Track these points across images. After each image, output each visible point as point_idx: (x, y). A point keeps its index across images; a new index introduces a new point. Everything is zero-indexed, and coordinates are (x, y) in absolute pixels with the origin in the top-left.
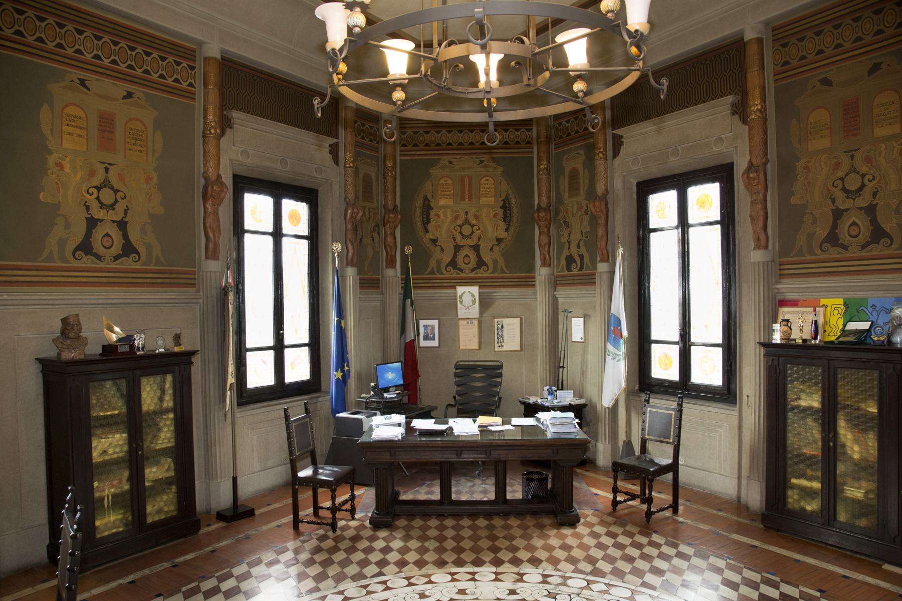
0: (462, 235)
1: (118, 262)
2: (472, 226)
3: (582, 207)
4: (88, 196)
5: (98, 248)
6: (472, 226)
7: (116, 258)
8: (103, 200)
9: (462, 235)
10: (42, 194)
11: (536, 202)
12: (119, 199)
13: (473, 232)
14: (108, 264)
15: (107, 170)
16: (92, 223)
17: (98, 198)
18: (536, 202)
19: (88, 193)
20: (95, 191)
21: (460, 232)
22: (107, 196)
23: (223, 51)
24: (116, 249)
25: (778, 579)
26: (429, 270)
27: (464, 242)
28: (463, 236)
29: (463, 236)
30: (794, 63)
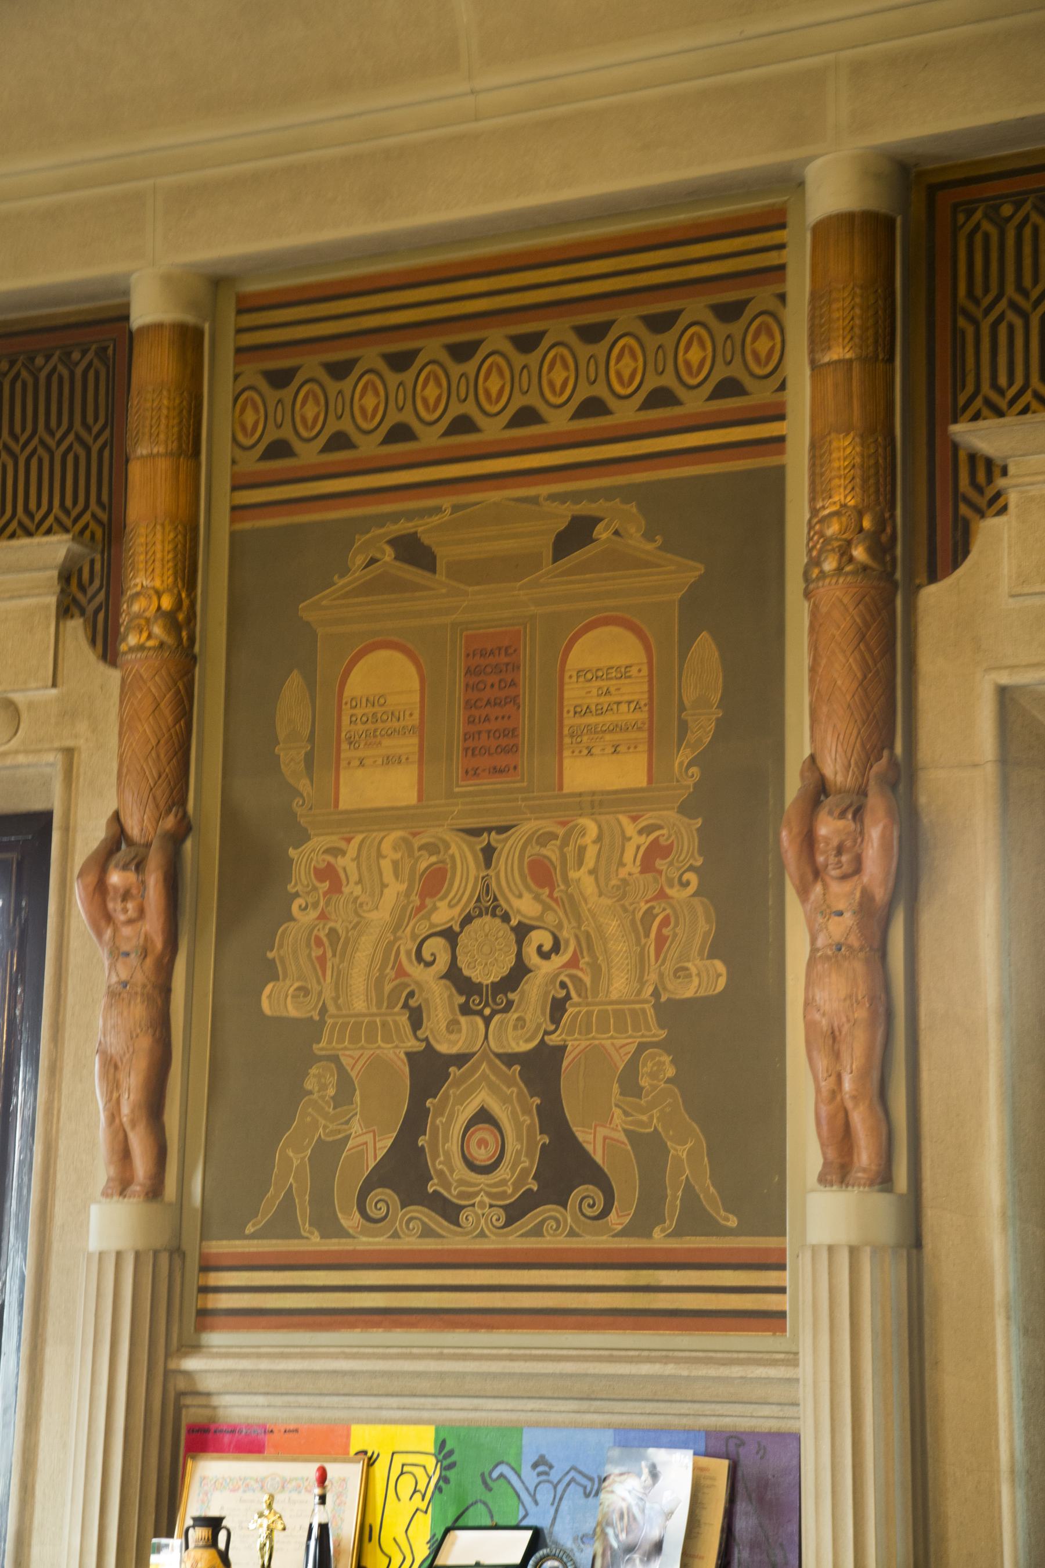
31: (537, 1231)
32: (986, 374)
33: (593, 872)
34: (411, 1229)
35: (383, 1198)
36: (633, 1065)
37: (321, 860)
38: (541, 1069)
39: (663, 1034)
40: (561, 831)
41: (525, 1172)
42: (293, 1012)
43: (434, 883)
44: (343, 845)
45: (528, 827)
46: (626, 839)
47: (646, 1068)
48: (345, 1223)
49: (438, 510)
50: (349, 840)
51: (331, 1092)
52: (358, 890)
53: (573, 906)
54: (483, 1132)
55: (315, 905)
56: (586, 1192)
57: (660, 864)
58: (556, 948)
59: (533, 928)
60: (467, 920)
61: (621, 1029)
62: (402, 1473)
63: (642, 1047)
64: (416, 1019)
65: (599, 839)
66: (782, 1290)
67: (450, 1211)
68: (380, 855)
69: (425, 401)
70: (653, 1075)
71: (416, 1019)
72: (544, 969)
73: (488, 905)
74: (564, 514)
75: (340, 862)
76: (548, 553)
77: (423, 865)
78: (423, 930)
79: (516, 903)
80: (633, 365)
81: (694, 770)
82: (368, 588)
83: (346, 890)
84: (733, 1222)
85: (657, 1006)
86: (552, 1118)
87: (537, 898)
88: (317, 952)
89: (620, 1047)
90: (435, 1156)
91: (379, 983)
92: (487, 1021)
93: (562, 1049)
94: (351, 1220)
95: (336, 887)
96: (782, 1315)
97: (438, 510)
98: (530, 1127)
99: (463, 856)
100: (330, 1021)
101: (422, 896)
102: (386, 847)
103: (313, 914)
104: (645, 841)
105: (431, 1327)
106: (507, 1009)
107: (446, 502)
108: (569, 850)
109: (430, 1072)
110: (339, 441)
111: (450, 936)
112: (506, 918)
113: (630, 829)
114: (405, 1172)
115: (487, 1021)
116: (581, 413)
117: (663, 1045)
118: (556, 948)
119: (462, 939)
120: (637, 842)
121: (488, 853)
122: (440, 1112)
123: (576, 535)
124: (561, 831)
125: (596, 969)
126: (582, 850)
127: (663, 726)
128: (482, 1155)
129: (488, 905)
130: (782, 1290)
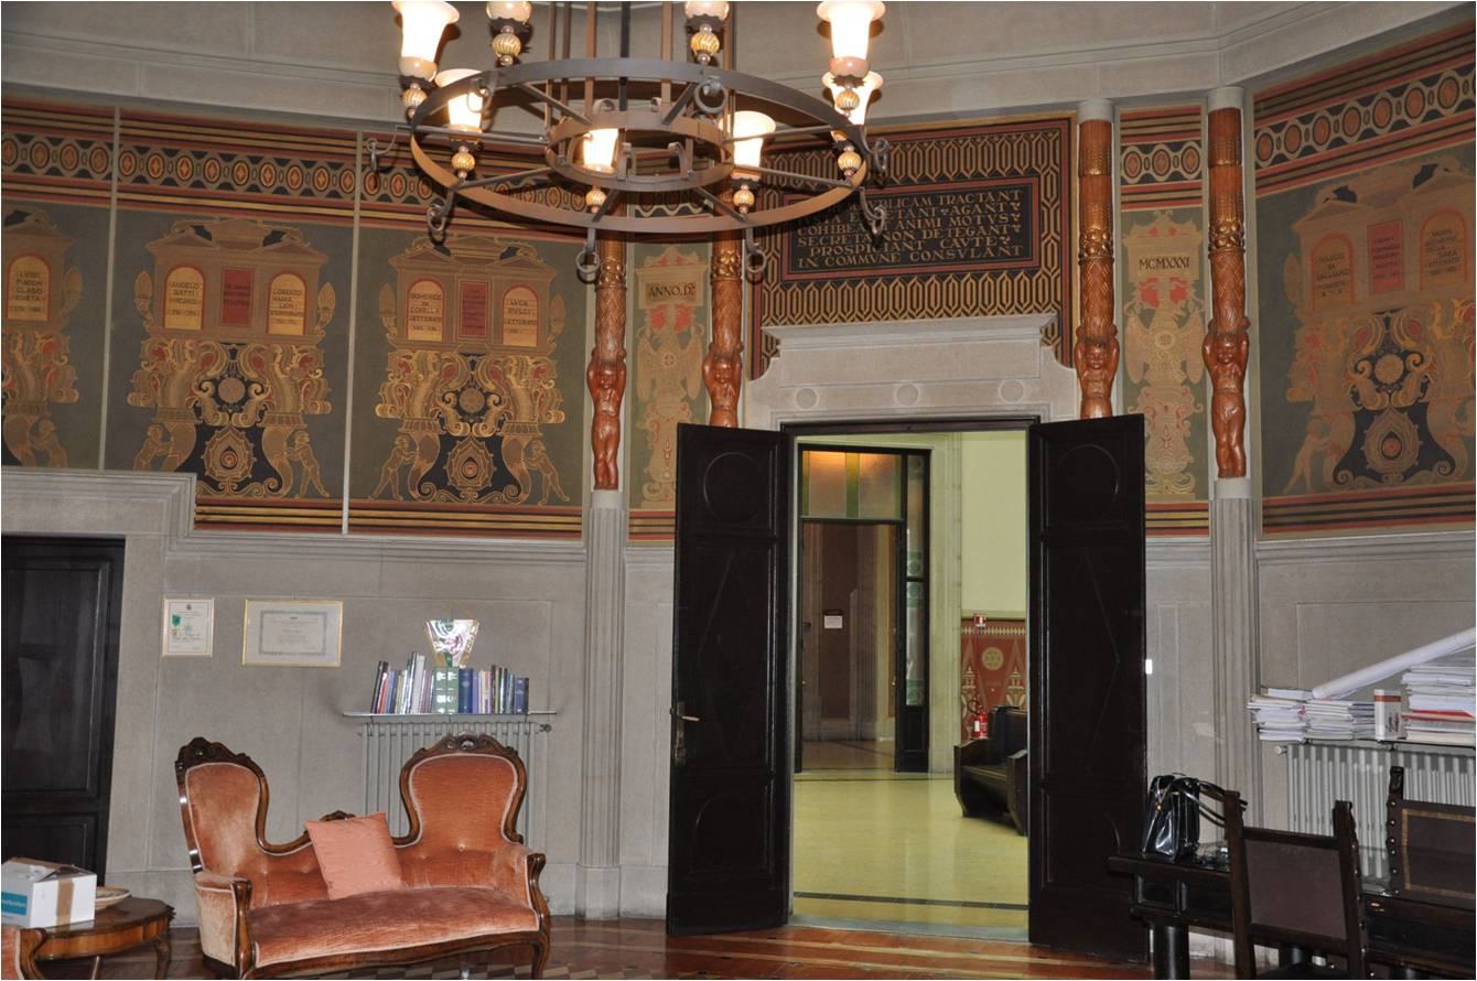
0: (1376, 381)
1: (1413, 479)
2: (1404, 355)
3: (700, 331)
4: (442, 405)
5: (1374, 458)
6: (1404, 355)
7: (1407, 475)
8: (1380, 378)
9: (1376, 381)
10: (379, 406)
11: (590, 344)
12: (491, 403)
13: (1406, 372)
14: (1392, 485)
15: (1387, 322)
16: (1364, 418)
17: (1372, 377)
18: (590, 344)
19: (444, 400)
20: (1365, 364)
21: (1372, 377)
22: (1390, 368)
23: (1114, 104)
24: (1409, 458)
25: (511, 966)
26: (1293, 481)
27: (219, 419)
28: (1380, 386)
29: (1380, 386)
30: (68, 176)
31: (490, 501)
32: (773, 245)
33: (515, 375)
34: (441, 497)
35: (428, 486)
36: (529, 445)
37: (156, 347)
38: (254, 434)
39: (305, 426)
40: (502, 360)
41: (246, 471)
42: (390, 416)
43: (208, 361)
44: (412, 354)
45: (252, 347)
46: (294, 354)
47: (534, 447)
48: (413, 495)
49: (212, 218)
50: (169, 340)
51: (160, 436)
52: (173, 360)
53: (508, 387)
54: (471, 464)
55: (399, 377)
56: (511, 489)
57: (307, 364)
58: (500, 402)
59: (253, 382)
60: (463, 389)
61: (288, 423)
62: (1256, 566)
63: (296, 430)
64: (442, 421)
65: (517, 365)
66: (1207, 519)
67: (457, 493)
68: (184, 348)
69: (182, 172)
70: (300, 440)
71: (442, 421)
72: (496, 410)
73: (472, 383)
74: (269, 229)
75: (410, 361)
76: (261, 243)
77: (445, 366)
78: (202, 377)
79: (486, 385)
80: (129, 164)
81: (554, 344)
82: (181, 242)
83: (167, 359)
84: (328, 495)
85: (304, 416)
86: (498, 461)
87: (256, 371)
88: (399, 394)
89: (287, 430)
90: (208, 463)
91: (427, 409)
92: (471, 425)
93: (502, 438)
94: (416, 494)
95: (408, 370)
96: (1207, 528)
97: (212, 218)
98: (249, 455)
99: (462, 364)
100: (406, 421)
101: (203, 365)
102: (187, 345)
103: (152, 368)
104: (301, 356)
105: (249, 529)
106: (481, 421)
107: (217, 216)
108: (11, 342)
109: (205, 433)
110: (169, 182)
111: (216, 382)
112: (481, 390)
113: (530, 362)
114: (438, 477)
115: (471, 425)
116: (277, 192)
117: (306, 430)
118: (500, 402)
119: (462, 397)
120: (40, 342)
121: (473, 365)
122: (211, 446)
123: (275, 237)
124: (502, 360)
125: (516, 411)
126: (15, 342)
127: (310, 316)
128: (470, 473)
129: (472, 383)
130: (579, 524)
